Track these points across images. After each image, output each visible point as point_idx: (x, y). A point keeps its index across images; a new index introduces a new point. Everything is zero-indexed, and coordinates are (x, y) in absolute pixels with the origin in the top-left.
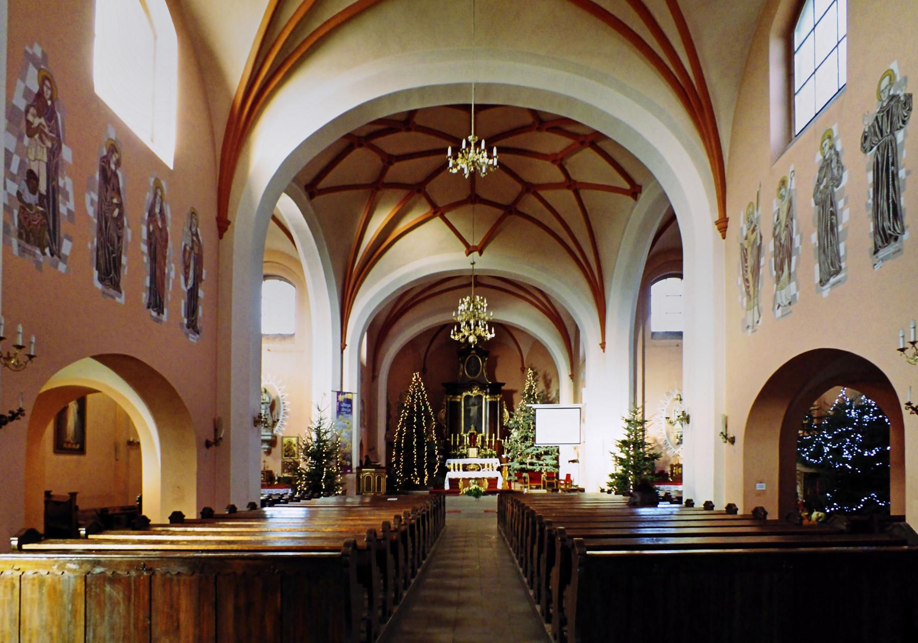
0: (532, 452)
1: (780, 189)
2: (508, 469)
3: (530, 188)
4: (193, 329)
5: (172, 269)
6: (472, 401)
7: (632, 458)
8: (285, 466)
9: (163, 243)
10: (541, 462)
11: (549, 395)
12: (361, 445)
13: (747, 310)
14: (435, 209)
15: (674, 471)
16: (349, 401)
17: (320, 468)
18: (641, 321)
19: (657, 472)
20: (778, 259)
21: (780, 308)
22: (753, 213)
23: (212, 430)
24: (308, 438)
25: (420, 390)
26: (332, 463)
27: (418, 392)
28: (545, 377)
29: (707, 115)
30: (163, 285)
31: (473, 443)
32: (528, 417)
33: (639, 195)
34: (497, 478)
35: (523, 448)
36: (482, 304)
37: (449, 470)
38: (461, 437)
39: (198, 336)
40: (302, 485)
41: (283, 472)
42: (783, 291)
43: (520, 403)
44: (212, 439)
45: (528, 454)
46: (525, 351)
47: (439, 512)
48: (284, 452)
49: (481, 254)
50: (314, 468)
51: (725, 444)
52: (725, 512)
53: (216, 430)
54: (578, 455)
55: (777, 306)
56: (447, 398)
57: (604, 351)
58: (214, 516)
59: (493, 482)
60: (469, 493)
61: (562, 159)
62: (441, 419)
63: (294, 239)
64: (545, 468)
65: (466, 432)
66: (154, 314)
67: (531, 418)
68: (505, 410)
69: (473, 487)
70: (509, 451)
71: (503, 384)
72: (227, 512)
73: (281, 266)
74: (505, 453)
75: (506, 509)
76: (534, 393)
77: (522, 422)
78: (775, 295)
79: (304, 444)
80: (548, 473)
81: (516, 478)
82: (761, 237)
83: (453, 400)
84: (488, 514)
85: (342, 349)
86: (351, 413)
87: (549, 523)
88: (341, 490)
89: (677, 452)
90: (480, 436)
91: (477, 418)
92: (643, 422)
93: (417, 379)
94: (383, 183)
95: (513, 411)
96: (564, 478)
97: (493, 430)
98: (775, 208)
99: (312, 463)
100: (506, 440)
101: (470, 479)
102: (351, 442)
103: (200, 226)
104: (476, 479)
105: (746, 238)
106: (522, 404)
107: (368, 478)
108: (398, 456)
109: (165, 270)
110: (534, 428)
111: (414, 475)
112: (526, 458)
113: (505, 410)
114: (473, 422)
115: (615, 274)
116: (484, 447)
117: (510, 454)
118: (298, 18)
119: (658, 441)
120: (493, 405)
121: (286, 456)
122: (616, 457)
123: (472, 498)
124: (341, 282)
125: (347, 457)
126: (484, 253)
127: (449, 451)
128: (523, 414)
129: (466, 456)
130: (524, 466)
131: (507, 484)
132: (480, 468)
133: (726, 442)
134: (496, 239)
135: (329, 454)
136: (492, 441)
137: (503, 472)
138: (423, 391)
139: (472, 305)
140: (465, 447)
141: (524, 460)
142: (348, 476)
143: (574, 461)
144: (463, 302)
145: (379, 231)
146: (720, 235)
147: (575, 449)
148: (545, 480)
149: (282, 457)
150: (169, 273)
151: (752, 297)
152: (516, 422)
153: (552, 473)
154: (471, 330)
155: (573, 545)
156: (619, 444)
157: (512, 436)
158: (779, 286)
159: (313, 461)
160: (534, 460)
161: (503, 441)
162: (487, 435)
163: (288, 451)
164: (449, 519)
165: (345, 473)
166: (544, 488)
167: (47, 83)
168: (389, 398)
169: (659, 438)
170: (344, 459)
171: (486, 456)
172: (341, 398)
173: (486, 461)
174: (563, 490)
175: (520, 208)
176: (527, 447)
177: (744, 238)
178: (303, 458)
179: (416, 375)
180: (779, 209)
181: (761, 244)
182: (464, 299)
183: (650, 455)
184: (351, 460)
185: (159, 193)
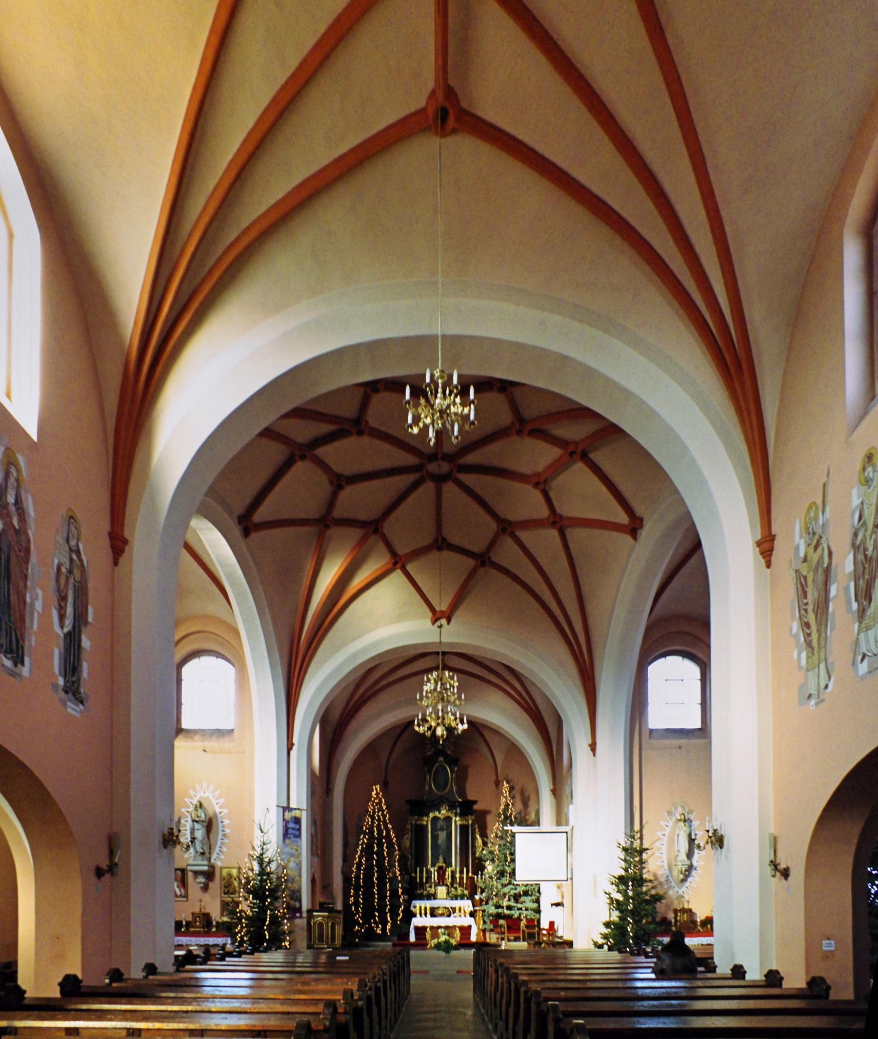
0: (509, 892)
1: (864, 469)
2: (483, 916)
3: (506, 527)
4: (74, 695)
5: (37, 599)
6: (440, 824)
7: (631, 901)
8: (225, 905)
9: (22, 554)
10: (519, 906)
11: (527, 817)
12: (313, 881)
13: (807, 670)
14: (394, 559)
15: (678, 918)
16: (297, 821)
17: (263, 910)
18: (637, 714)
19: (658, 919)
20: (861, 582)
21: (866, 660)
22: (816, 518)
23: (105, 852)
24: (249, 869)
25: (381, 809)
26: (277, 904)
27: (378, 812)
28: (522, 793)
29: (747, 375)
30: (22, 619)
31: (441, 881)
32: (504, 845)
33: (638, 532)
34: (470, 927)
35: (499, 887)
36: (452, 682)
37: (415, 916)
38: (428, 872)
39: (81, 707)
40: (241, 932)
41: (222, 915)
42: (871, 633)
43: (495, 828)
44: (104, 864)
45: (505, 895)
46: (500, 759)
47: (402, 978)
48: (223, 888)
49: (449, 622)
50: (257, 910)
51: (773, 879)
52: (730, 976)
53: (112, 853)
54: (563, 897)
55: (860, 657)
56: (412, 819)
57: (594, 755)
58: (83, 990)
59: (466, 931)
60: (438, 946)
61: (546, 481)
62: (405, 848)
63: (231, 602)
64: (525, 913)
65: (433, 865)
66: (8, 663)
67: (509, 845)
68: (478, 836)
69: (443, 938)
70: (482, 891)
71: (475, 802)
72: (107, 981)
73: (218, 638)
74: (478, 893)
75: (486, 972)
76: (511, 814)
77: (497, 851)
78: (858, 639)
79: (245, 878)
80: (528, 920)
81: (492, 927)
82: (830, 554)
83: (419, 822)
84: (460, 976)
85: (289, 750)
86: (299, 836)
87: (525, 983)
88: (288, 941)
89: (681, 892)
90: (449, 870)
91: (447, 846)
92: (641, 851)
93: (377, 794)
94: (333, 518)
95: (487, 837)
96: (547, 927)
97: (464, 863)
98: (856, 502)
99: (254, 904)
100: (479, 876)
101: (439, 927)
102: (300, 876)
103: (82, 538)
104: (447, 928)
105: (805, 560)
106: (498, 829)
107: (321, 924)
108: (356, 896)
109: (25, 596)
110: (513, 861)
111: (375, 922)
112: (503, 899)
113: (478, 836)
114: (441, 851)
115: (607, 651)
116: (455, 886)
117: (484, 895)
118: (206, 219)
119: (659, 877)
120: (464, 829)
121: (225, 893)
122: (611, 899)
123: (442, 953)
124: (286, 660)
125: (296, 895)
126: (453, 620)
127: (416, 891)
128: (498, 841)
129: (433, 896)
130: (500, 910)
131: (482, 934)
132: (450, 912)
133: (774, 876)
134: (468, 599)
135: (274, 892)
136: (463, 878)
137: (477, 918)
138: (384, 811)
139: (439, 683)
140: (433, 885)
141: (500, 902)
142: (297, 921)
143: (557, 905)
144: (429, 680)
145: (330, 587)
146: (763, 561)
147: (559, 888)
148: (525, 928)
149: (221, 894)
150: (32, 605)
151: (816, 649)
152: (491, 852)
153: (532, 920)
154: (438, 718)
155: (548, 1009)
156: (613, 880)
157: (486, 870)
158: (863, 625)
159: (255, 901)
160: (512, 903)
161: (476, 877)
162: (458, 869)
163: (228, 888)
164: (416, 982)
165: (294, 917)
166: (524, 940)
167: (72, 520)
168: (346, 819)
169: (660, 873)
170: (291, 899)
171: (456, 897)
172: (288, 815)
173: (457, 904)
174: (546, 943)
175: (495, 558)
176: (504, 886)
177: (802, 560)
178: (244, 896)
179: (376, 789)
180: (862, 503)
181: (830, 564)
182: (430, 676)
183: (652, 896)
184: (300, 901)
185: (13, 470)
